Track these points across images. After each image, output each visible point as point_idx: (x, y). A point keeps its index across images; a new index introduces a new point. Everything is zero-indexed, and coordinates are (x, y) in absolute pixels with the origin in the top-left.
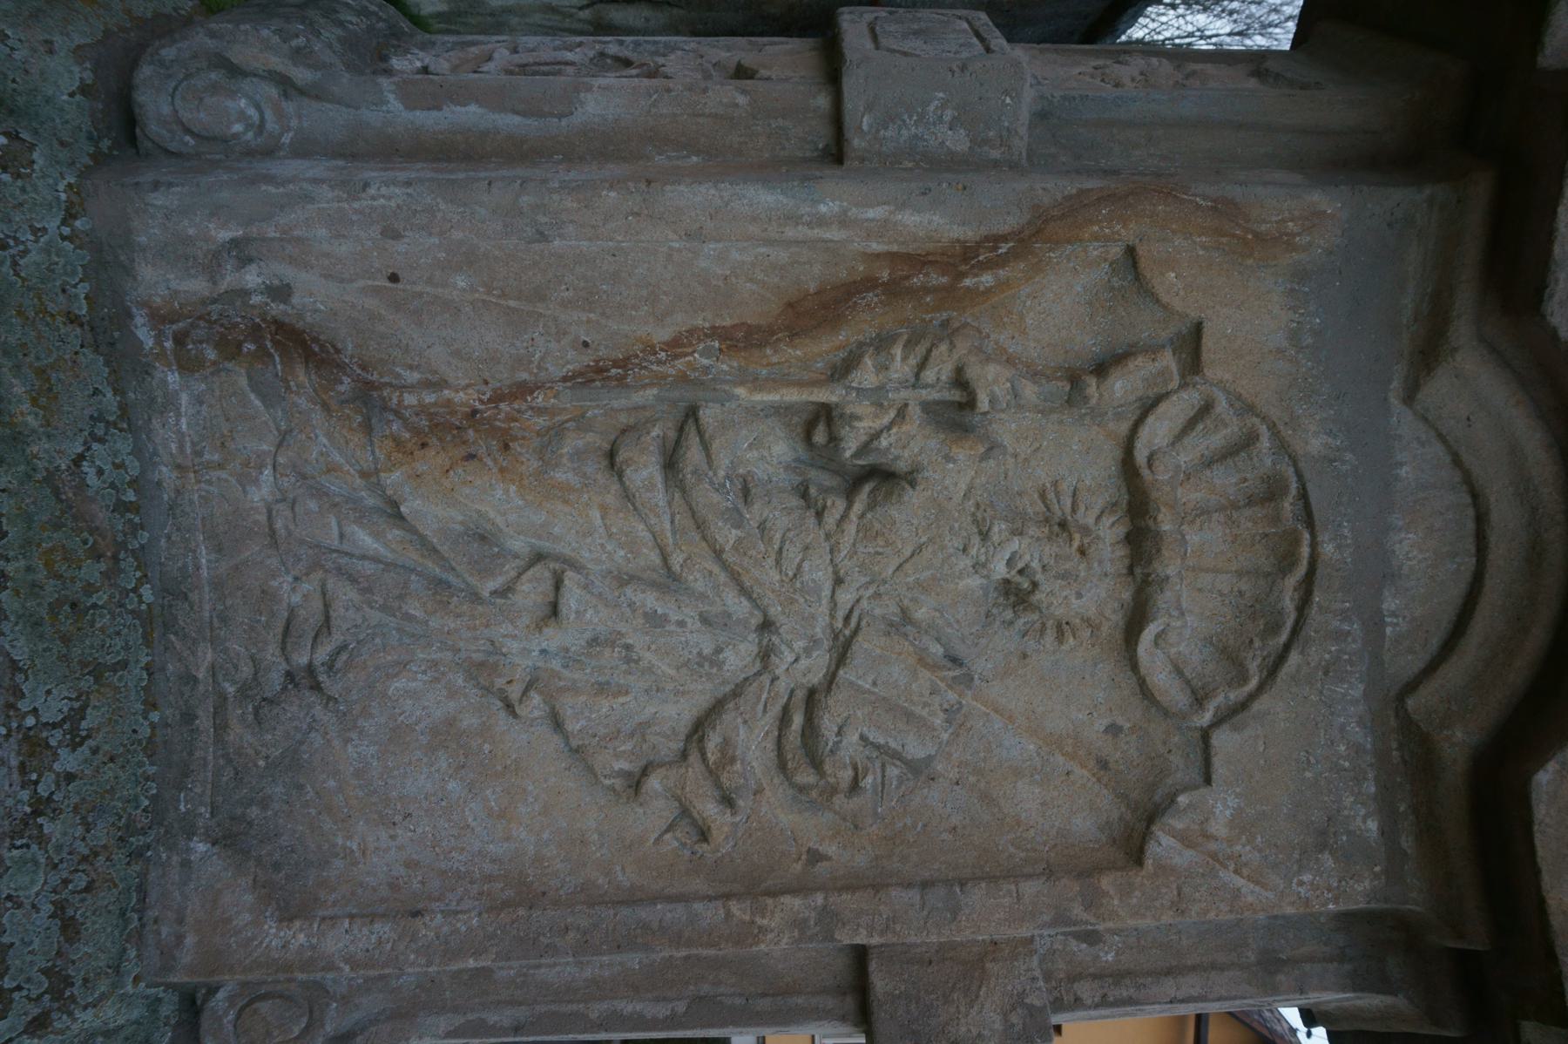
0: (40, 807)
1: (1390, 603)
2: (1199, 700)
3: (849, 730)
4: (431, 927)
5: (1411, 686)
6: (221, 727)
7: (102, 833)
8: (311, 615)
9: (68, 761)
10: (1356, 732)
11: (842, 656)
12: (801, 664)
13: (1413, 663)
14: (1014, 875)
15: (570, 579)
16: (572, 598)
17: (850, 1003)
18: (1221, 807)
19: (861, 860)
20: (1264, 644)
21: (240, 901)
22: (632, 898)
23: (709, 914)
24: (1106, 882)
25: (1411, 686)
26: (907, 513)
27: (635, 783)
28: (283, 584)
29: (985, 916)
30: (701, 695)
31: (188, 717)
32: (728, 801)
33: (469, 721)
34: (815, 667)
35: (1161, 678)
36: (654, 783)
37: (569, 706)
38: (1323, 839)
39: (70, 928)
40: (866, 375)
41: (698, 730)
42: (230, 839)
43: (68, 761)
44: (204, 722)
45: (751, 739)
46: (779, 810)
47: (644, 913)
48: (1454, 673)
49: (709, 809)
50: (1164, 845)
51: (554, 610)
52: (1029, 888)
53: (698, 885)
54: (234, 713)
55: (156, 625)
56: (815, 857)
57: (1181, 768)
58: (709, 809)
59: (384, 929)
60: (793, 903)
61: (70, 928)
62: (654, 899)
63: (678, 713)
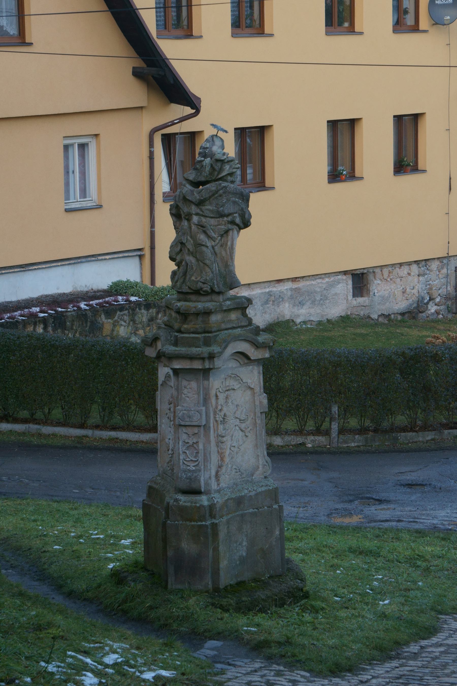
0: (254, 490)
1: (234, 366)
2: (240, 383)
3: (243, 417)
4: (259, 454)
5: (241, 364)
6: (244, 478)
7: (254, 485)
8: (235, 470)
9: (250, 489)
10: (244, 369)
11: (237, 418)
12: (238, 422)
13: (238, 364)
14: (254, 400)
15: (232, 445)
16: (234, 445)
17: (164, 26)
18: (249, 381)
19: (252, 414)
20: (236, 377)
21: (258, 473)
22: (256, 435)
23: (258, 428)
24: (255, 392)
25: (241, 364)
26: (228, 414)
27: (247, 436)
28: (233, 473)
29: (257, 403)
30: (240, 431)
31: (243, 481)
32: (248, 428)
33: (241, 454)
34: (238, 420)
35: (238, 386)
36: (247, 435)
37: (240, 444)
38: (252, 371)
39: (262, 486)
40: (218, 419)
41: (242, 431)
42: (253, 475)
43: (250, 489)
44: (243, 479)
45: (243, 426)
46: (248, 422)
47: (258, 434)
48: (240, 360)
49: (249, 429)
50: (252, 386)
51: (234, 446)
52: (256, 399)
53: (255, 430)
54: (243, 476)
55: (237, 485)
56: (252, 418)
57: (246, 384)
58: (249, 429)
59: (260, 458)
60: (257, 420)
61: (262, 486)
62: (256, 433)
63: (241, 433)
